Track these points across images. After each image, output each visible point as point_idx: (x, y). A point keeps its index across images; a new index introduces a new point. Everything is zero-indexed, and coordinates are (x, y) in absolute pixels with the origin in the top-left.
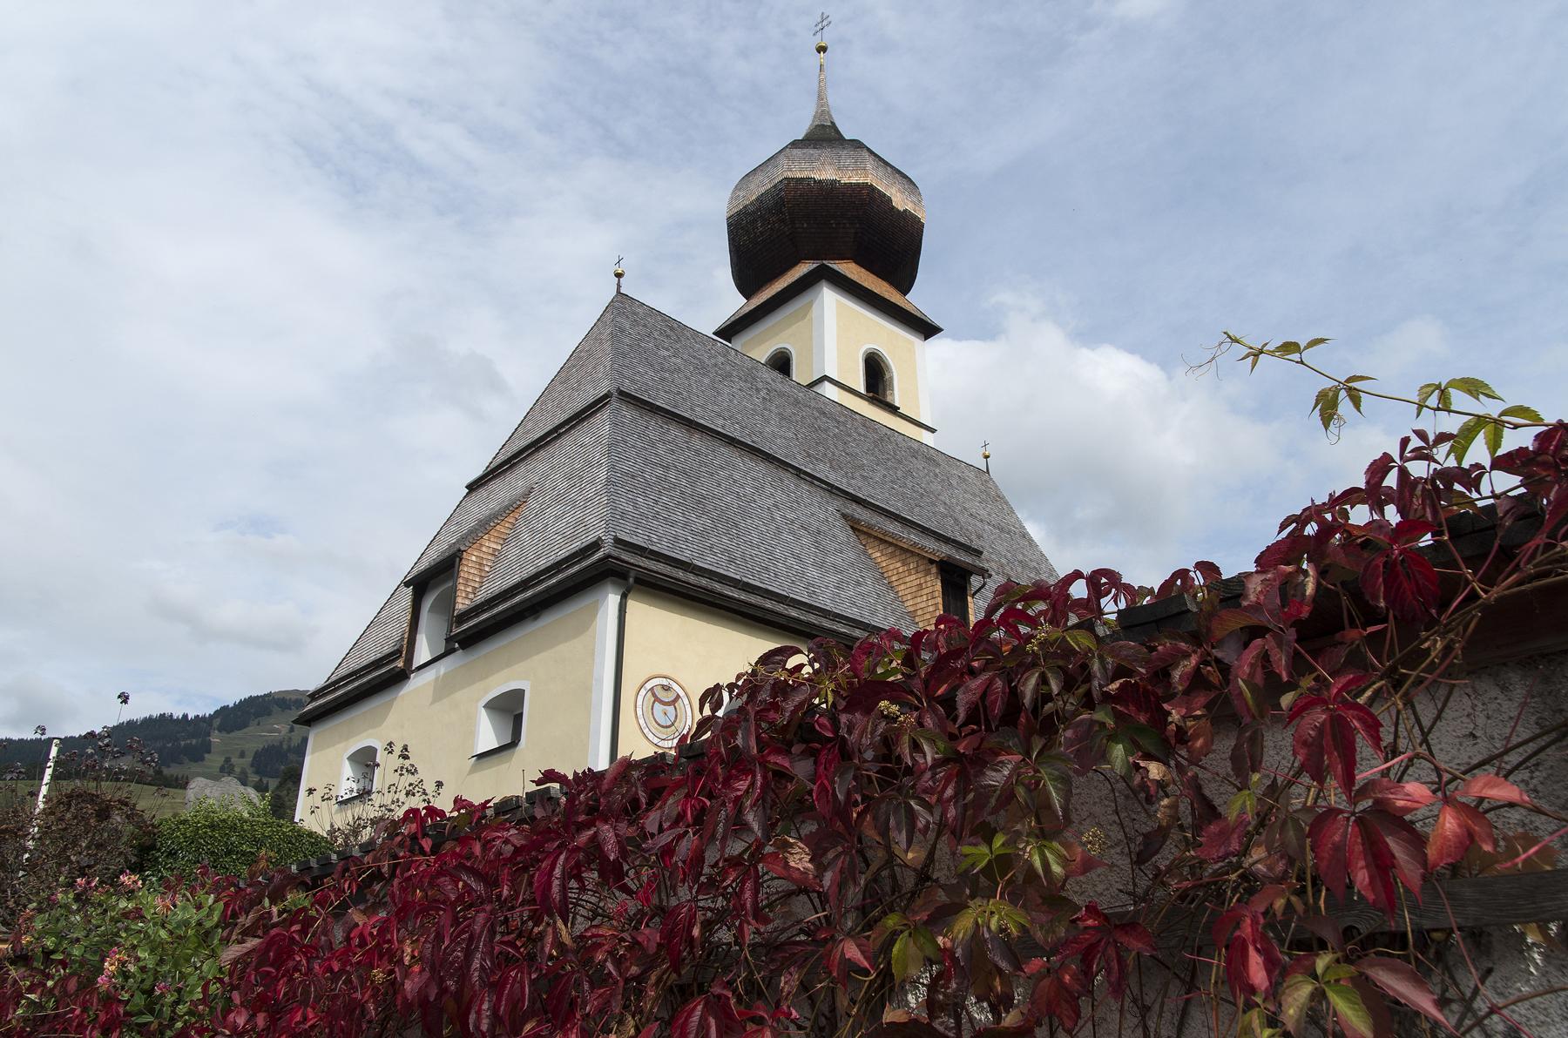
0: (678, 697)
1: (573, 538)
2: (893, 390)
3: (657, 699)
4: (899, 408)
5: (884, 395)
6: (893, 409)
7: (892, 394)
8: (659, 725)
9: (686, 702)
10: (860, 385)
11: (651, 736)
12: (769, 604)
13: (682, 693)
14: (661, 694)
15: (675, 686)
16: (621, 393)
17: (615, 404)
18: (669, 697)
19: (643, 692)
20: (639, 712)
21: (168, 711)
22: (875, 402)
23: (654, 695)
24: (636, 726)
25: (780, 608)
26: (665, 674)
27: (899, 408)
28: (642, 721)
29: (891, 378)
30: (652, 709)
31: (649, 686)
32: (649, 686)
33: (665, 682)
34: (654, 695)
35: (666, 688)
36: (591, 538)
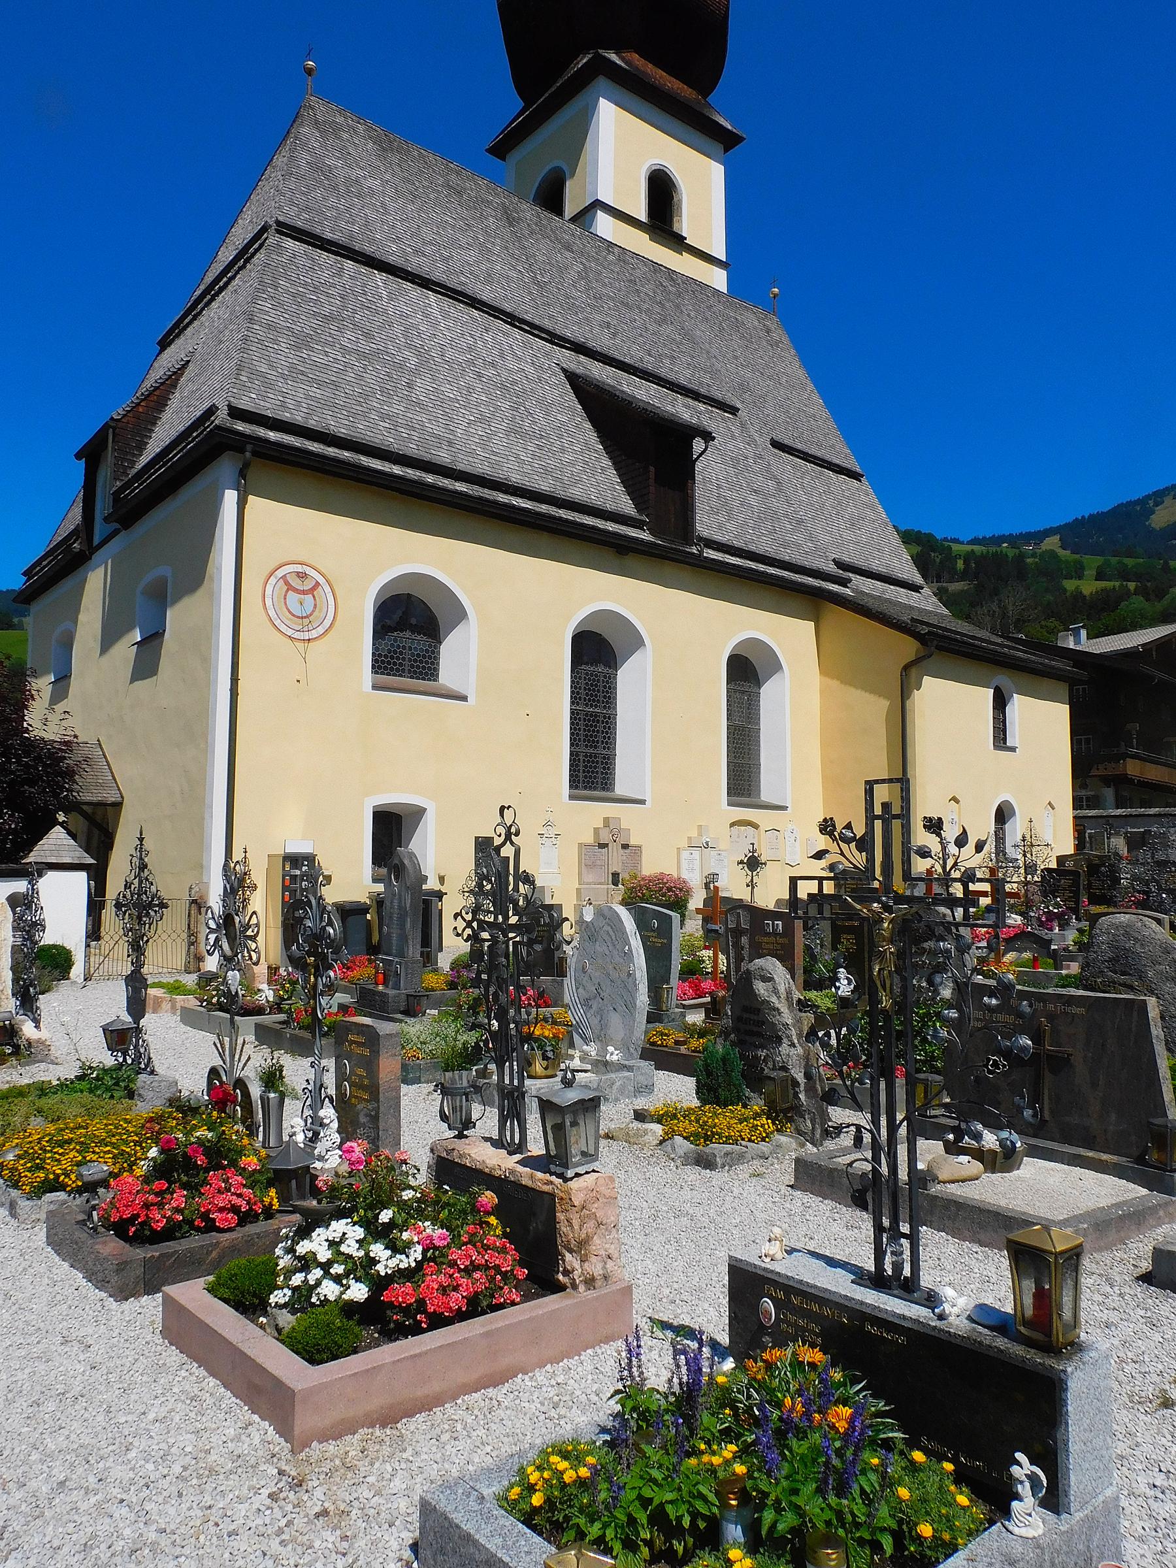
0: (318, 584)
1: (573, 409)
2: (681, 216)
3: (290, 588)
4: (686, 239)
5: (671, 225)
6: (678, 242)
7: (680, 221)
8: (294, 615)
9: (327, 589)
10: (641, 212)
11: (283, 628)
12: (430, 478)
13: (321, 580)
14: (296, 583)
15: (309, 571)
16: (278, 223)
17: (272, 239)
18: (308, 585)
19: (273, 580)
20: (269, 602)
21: (1120, 502)
22: (657, 231)
23: (287, 583)
24: (266, 619)
25: (445, 483)
26: (300, 559)
27: (686, 239)
28: (272, 613)
29: (680, 201)
30: (285, 599)
31: (280, 573)
32: (280, 573)
33: (299, 568)
34: (287, 583)
35: (302, 576)
36: (206, 405)
